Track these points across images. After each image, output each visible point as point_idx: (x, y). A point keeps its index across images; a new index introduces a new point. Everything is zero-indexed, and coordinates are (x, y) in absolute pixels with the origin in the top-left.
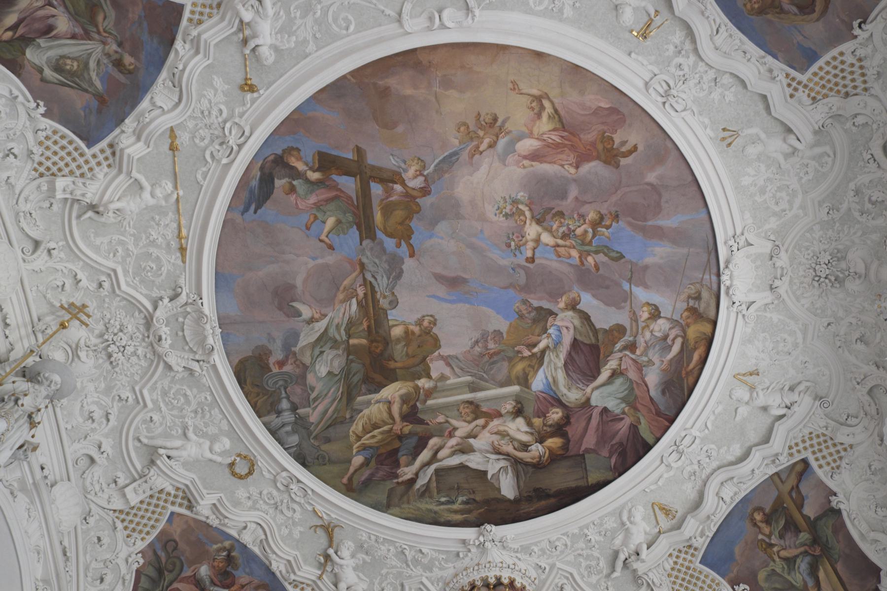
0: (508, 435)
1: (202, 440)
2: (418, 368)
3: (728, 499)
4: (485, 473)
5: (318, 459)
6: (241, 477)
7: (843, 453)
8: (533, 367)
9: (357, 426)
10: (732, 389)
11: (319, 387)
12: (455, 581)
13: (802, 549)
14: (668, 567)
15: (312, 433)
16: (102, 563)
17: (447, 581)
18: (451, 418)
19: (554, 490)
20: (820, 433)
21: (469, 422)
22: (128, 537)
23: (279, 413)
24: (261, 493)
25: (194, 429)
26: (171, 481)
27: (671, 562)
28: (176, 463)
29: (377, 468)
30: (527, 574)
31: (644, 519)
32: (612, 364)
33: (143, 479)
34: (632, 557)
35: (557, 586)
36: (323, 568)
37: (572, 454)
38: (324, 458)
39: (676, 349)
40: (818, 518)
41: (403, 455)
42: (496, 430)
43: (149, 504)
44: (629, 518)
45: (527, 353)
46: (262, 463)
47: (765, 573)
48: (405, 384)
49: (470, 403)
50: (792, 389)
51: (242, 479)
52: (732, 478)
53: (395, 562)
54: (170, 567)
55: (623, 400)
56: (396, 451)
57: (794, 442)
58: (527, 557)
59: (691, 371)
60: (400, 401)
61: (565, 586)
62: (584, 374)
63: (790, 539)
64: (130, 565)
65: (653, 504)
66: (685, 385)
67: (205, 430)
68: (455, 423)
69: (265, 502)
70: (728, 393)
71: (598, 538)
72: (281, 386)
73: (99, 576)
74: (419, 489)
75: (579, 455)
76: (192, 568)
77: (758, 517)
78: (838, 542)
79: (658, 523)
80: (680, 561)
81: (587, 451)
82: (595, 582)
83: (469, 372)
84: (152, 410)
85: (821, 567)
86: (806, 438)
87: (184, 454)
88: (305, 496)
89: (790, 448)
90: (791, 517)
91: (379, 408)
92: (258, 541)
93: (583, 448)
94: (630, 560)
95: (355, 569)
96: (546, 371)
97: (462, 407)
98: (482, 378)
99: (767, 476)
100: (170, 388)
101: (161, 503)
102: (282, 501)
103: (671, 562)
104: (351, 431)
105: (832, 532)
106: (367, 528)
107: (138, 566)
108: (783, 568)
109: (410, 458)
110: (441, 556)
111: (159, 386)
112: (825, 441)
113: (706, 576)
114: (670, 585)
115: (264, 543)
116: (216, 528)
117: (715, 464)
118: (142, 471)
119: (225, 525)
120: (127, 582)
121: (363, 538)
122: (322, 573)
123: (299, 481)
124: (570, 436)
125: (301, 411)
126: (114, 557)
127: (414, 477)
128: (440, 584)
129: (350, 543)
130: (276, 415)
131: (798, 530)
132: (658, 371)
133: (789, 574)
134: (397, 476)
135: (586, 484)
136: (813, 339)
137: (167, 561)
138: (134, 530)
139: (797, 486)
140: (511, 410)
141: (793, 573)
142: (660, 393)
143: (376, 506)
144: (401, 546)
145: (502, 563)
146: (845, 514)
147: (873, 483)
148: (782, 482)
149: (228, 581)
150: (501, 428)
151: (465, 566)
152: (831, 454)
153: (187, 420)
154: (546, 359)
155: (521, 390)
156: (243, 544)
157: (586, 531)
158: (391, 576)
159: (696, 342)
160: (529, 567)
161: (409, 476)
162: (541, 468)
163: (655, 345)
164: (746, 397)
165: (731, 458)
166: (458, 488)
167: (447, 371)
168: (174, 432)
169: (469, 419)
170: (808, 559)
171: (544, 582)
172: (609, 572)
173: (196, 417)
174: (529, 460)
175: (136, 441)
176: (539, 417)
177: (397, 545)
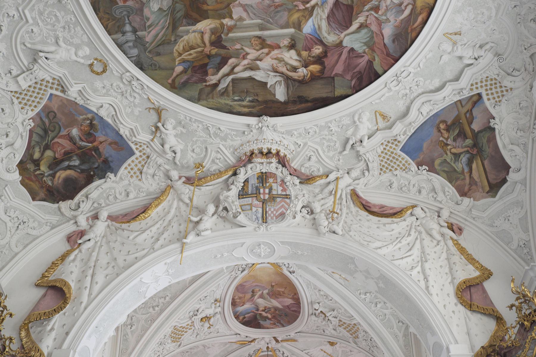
0: (284, 61)
1: (69, 47)
2: (224, 11)
3: (425, 114)
4: (266, 84)
5: (151, 66)
6: (98, 74)
7: (505, 93)
8: (305, 17)
9: (179, 46)
10: (441, 43)
11: (152, 18)
12: (241, 148)
13: (466, 149)
14: (379, 151)
15: (147, 48)
16: (6, 125)
17: (236, 148)
18: (246, 47)
19: (311, 98)
20: (493, 78)
21: (258, 50)
22: (22, 109)
23: (124, 33)
24: (112, 85)
25: (63, 39)
26: (49, 73)
27: (382, 148)
28: (52, 62)
29: (192, 75)
30: (288, 148)
31: (368, 120)
32: (361, 19)
33: (30, 72)
34: (358, 144)
35: (307, 156)
36: (154, 134)
37: (326, 76)
38: (155, 65)
39: (407, 12)
40: (479, 132)
41: (210, 68)
42: (275, 57)
43: (35, 88)
44: (359, 119)
45: (302, 7)
46: (112, 65)
47: (440, 161)
48: (214, 22)
49: (259, 37)
50: (481, 47)
51: (99, 75)
52: (431, 100)
53: (202, 134)
54: (52, 129)
55: (365, 44)
56: (206, 65)
57: (475, 81)
58: (289, 137)
59: (415, 28)
60: (210, 33)
61: (312, 157)
62: (340, 24)
63: (459, 141)
64: (25, 127)
65: (376, 111)
66: (410, 37)
67: (71, 40)
68: (247, 50)
69: (115, 91)
70: (438, 45)
71: (337, 129)
72: (125, 15)
73: (5, 133)
74: (220, 91)
75: (330, 77)
76: (67, 130)
77: (442, 126)
78: (489, 147)
79: (377, 124)
80: (388, 148)
81: (337, 75)
82: (331, 156)
83: (259, 17)
84: (32, 25)
85: (475, 161)
86: (484, 80)
87: (58, 57)
88: (142, 89)
89: (472, 85)
90: (463, 129)
91: (195, 36)
92: (111, 116)
93: (334, 73)
94: (356, 145)
95: (176, 136)
96: (314, 20)
97: (253, 39)
98: (268, 22)
99: (453, 102)
100: (45, 10)
101: (43, 88)
102: (126, 91)
103: (382, 148)
104: (174, 50)
105: (487, 141)
106: (183, 112)
107: (31, 127)
108: (452, 159)
109: (215, 70)
110: (233, 133)
111: (36, 8)
112: (495, 84)
113: (403, 159)
114: (379, 162)
115: (114, 117)
116: (82, 105)
117: (420, 91)
118: (28, 65)
119: (87, 104)
120: (24, 138)
121: (182, 118)
122: (154, 138)
123: (138, 79)
124: (326, 64)
125: (139, 33)
126: (14, 121)
127: (217, 82)
128: (231, 149)
129: (172, 120)
130: (122, 35)
131: (465, 137)
132: (392, 26)
133: (454, 163)
134: (206, 81)
135: (333, 96)
136: (502, 15)
137: (50, 125)
138: (26, 104)
139: (471, 110)
140: (287, 45)
141: (457, 163)
142: (391, 42)
143: (190, 99)
144: (206, 125)
145: (272, 140)
146: (497, 132)
147: (519, 114)
148: (462, 106)
149: (92, 139)
150: (280, 56)
151: (248, 140)
152: (497, 92)
153: (58, 33)
154: (315, 12)
155: (296, 32)
156: (100, 116)
157: (330, 125)
158: (199, 142)
159: (422, 9)
160: (290, 143)
161: (214, 82)
162: (304, 84)
163: (393, 9)
164: (449, 49)
165: (432, 88)
166: (247, 92)
167: (244, 15)
168: (49, 41)
169: (257, 48)
170: (468, 156)
171: (298, 153)
172: (341, 150)
173: (64, 31)
174: (296, 78)
175: (22, 45)
176: (306, 51)
177: (204, 124)
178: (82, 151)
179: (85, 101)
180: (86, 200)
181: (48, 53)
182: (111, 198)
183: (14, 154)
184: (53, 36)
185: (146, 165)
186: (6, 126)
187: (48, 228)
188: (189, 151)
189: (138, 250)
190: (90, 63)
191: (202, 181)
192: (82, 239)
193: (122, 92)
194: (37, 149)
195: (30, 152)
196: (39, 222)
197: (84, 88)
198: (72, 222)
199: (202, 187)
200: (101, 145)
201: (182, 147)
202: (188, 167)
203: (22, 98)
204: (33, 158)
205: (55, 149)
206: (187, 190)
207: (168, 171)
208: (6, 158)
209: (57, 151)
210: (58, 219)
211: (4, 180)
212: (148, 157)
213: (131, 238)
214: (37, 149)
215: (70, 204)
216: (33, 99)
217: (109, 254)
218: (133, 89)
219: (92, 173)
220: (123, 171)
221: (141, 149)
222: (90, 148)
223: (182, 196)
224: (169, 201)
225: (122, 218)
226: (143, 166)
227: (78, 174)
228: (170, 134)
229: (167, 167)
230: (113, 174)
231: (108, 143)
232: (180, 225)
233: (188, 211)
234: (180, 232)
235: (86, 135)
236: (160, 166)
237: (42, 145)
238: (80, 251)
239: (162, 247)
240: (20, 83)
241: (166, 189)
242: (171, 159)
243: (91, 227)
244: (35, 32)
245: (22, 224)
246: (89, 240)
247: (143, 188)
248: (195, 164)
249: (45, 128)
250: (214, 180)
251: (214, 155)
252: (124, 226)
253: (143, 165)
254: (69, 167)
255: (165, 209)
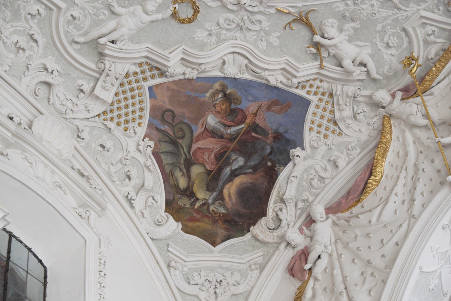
1: (132, 9)
6: (190, 21)
16: (120, 164)
22: (125, 130)
24: (218, 24)
33: (104, 74)
36: (318, 57)
43: (124, 92)
51: (193, 21)
53: (385, 13)
54: (180, 134)
64: (145, 154)
69: (227, 30)
73: (124, 176)
76: (200, 124)
84: (68, 9)
87: (124, 30)
92: (244, 68)
95: (350, 40)
101: (135, 85)
102: (243, 20)
107: (152, 149)
116: (197, 78)
118: (97, 67)
119: (204, 71)
120: (151, 167)
121: (341, 9)
122: (321, 62)
126: (125, 154)
129: (331, 20)
138: (127, 122)
149: (240, 117)
156: (231, 78)
158: (388, 27)
175: (73, 44)
178: (238, 142)
179: (197, 69)
180: (284, 205)
181: (110, 33)
182: (315, 182)
183: (153, 198)
184: (102, 6)
185: (336, 108)
186: (119, 165)
187: (256, 272)
188: (383, 50)
189: (394, 232)
190: (171, 12)
191: (427, 81)
192: (308, 261)
193: (238, 25)
194: (178, 174)
195: (172, 182)
196: (239, 271)
197: (185, 52)
198: (283, 246)
199: (432, 90)
200: (257, 118)
201: (369, 51)
202: (396, 74)
203: (118, 116)
204: (180, 189)
205: (201, 159)
206: (415, 106)
207: (370, 97)
208: (146, 209)
209: (206, 162)
210: (261, 253)
211: (161, 240)
212: (331, 95)
213: (374, 220)
214: (178, 174)
215: (266, 224)
216: (131, 109)
217: (356, 261)
218: (248, 11)
219: (269, 164)
220: (309, 135)
221: (314, 89)
222: (246, 130)
223: (413, 119)
224: (398, 138)
225: (346, 200)
226: (332, 112)
227: (252, 176)
228: (340, 43)
229: (366, 92)
230: (298, 149)
231: (264, 109)
232: (433, 161)
233: (433, 136)
234: (439, 171)
235: (229, 115)
236: (355, 97)
237: (180, 163)
238: (316, 279)
239: (424, 206)
240: (101, 98)
241: (383, 124)
242: (364, 77)
243: (312, 238)
244: (77, 17)
245: (218, 286)
246: (319, 257)
247: (351, 143)
248: (402, 62)
249: (170, 138)
250: (443, 67)
251: (421, 32)
252: (356, 210)
253: (331, 111)
254: (234, 174)
255: (398, 153)
